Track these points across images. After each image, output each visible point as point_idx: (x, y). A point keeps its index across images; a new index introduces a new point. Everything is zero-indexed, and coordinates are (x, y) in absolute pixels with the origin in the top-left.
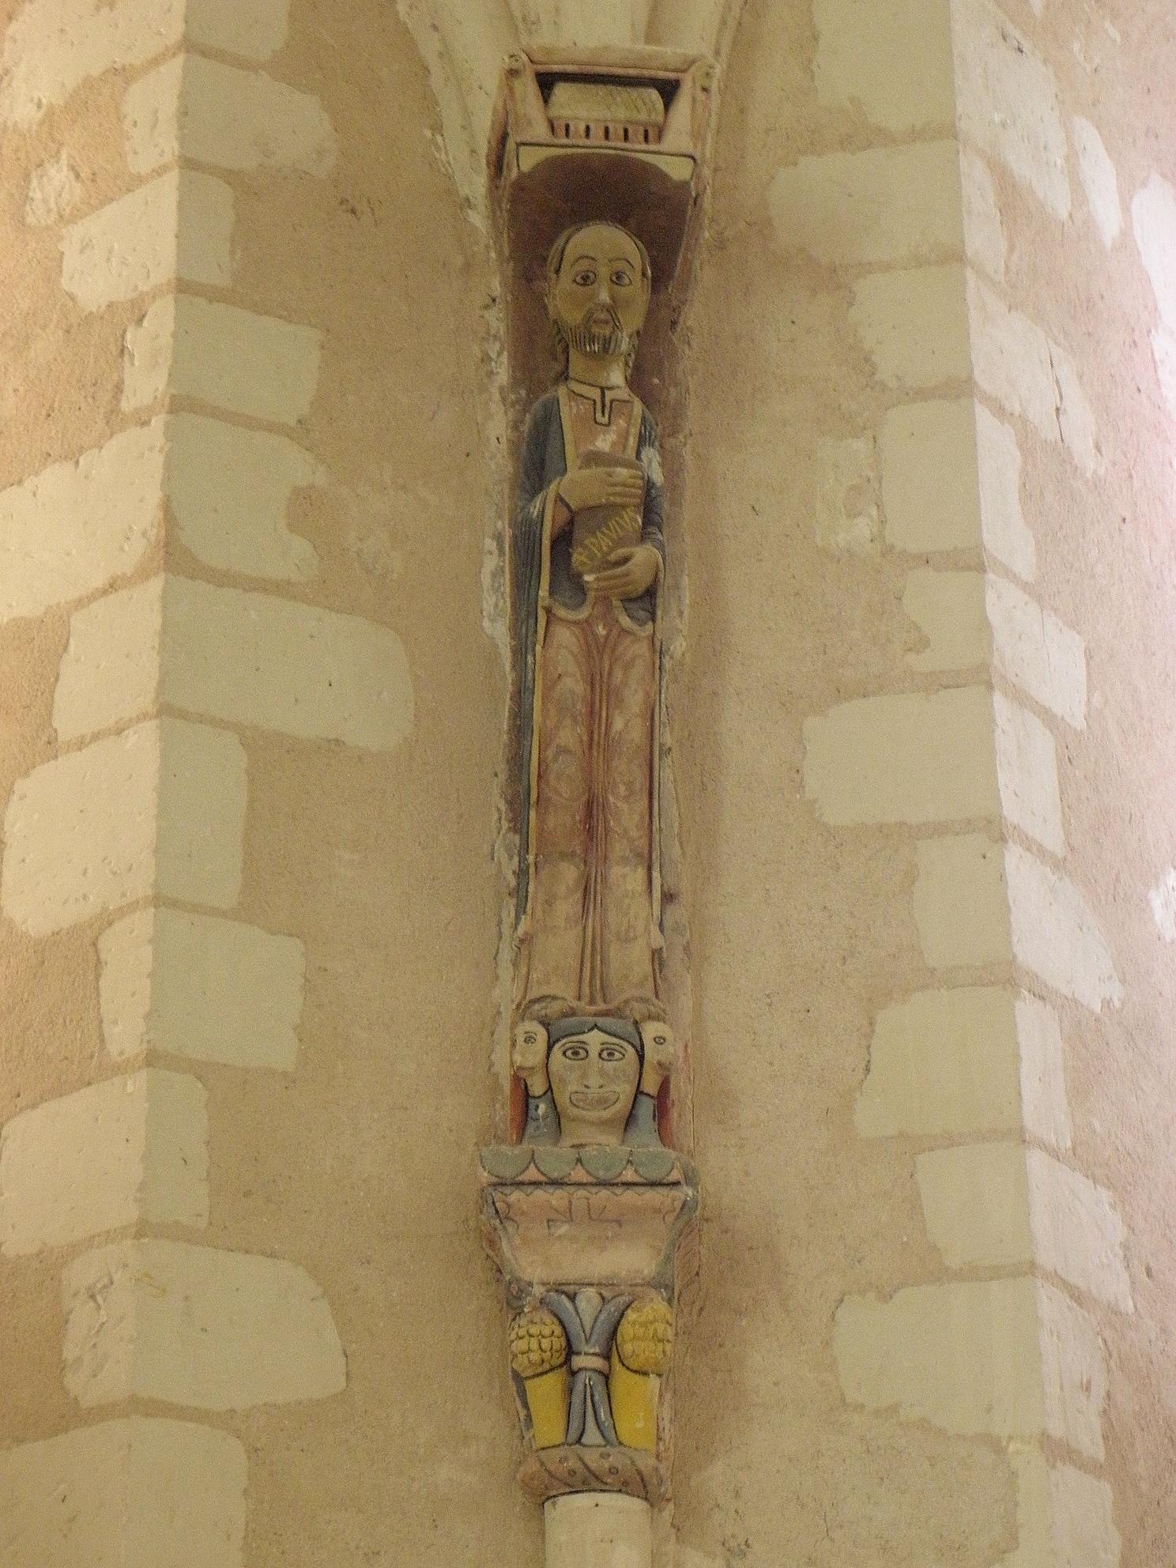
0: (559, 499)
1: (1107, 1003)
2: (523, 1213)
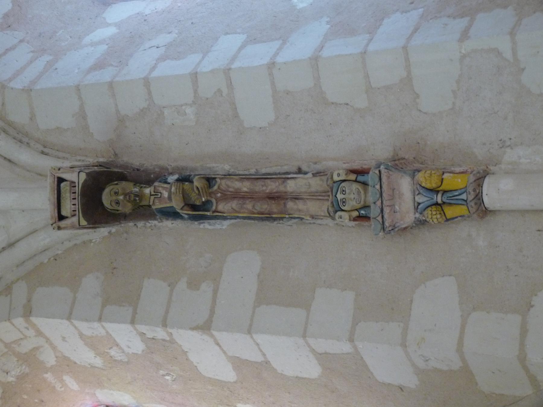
0: (182, 209)
1: (328, 23)
2: (393, 221)
